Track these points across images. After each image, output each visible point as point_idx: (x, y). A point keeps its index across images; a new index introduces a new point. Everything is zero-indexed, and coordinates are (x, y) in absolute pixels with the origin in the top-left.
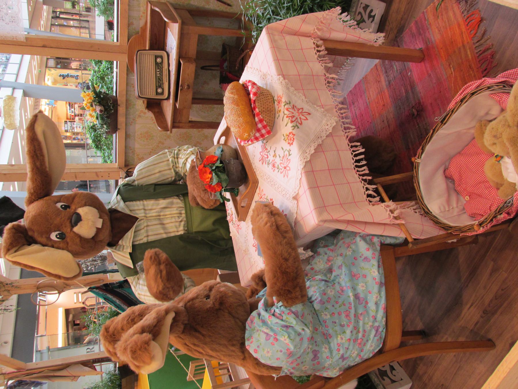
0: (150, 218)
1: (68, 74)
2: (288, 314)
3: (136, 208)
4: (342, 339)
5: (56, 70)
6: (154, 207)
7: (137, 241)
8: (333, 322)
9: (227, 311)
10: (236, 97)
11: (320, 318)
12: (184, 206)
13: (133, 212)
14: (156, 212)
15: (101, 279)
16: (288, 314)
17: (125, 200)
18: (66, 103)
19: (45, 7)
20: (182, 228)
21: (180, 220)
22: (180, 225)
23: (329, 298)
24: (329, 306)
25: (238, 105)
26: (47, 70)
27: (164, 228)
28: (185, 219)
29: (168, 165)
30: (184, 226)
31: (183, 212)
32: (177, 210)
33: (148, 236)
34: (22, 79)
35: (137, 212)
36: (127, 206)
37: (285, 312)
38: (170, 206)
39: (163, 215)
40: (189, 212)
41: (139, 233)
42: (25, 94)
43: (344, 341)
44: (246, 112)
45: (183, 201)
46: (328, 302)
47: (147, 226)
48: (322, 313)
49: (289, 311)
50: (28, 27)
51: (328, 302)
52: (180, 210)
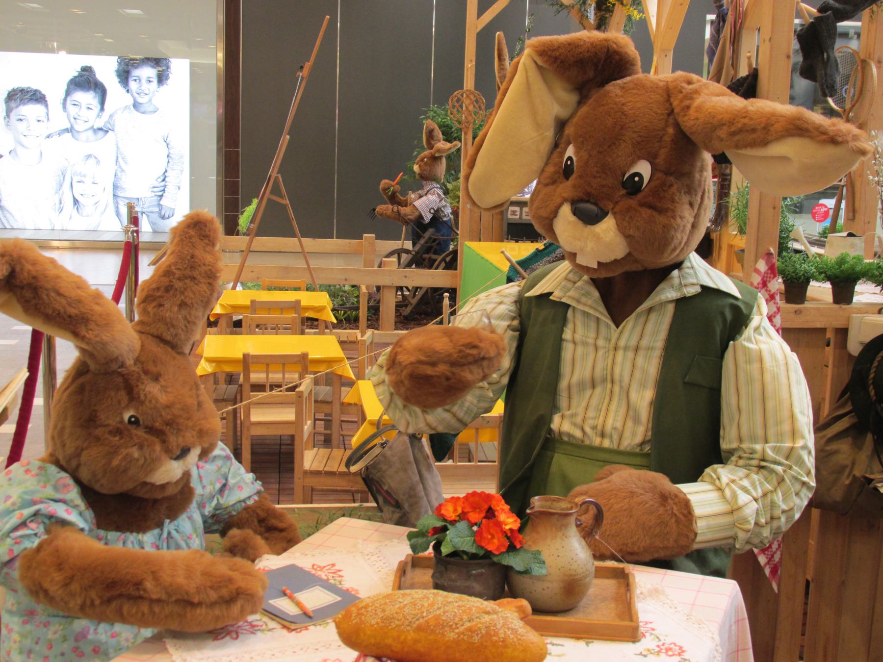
0: (611, 357)
2: (11, 551)
3: (650, 326)
4: (15, 642)
6: (638, 374)
7: (574, 316)
8: (39, 639)
9: (85, 445)
10: (452, 636)
11: (57, 619)
12: (622, 448)
13: (642, 320)
14: (621, 376)
15: (857, 216)
16: (11, 551)
17: (682, 303)
20: (566, 427)
21: (588, 429)
22: (575, 425)
23: (82, 655)
24: (66, 647)
25: (419, 629)
27: (581, 386)
28: (587, 442)
29: (754, 439)
30: (569, 435)
31: (606, 444)
32: (615, 428)
33: (574, 343)
35: (638, 329)
36: (663, 304)
37: (17, 546)
38: (631, 413)
39: (612, 391)
40: (602, 456)
41: (593, 325)
43: (12, 644)
44: (389, 641)
45: (638, 450)
46: (75, 650)
47: (596, 348)
48: (61, 627)
49: (16, 553)
51: (75, 650)
52: (611, 437)
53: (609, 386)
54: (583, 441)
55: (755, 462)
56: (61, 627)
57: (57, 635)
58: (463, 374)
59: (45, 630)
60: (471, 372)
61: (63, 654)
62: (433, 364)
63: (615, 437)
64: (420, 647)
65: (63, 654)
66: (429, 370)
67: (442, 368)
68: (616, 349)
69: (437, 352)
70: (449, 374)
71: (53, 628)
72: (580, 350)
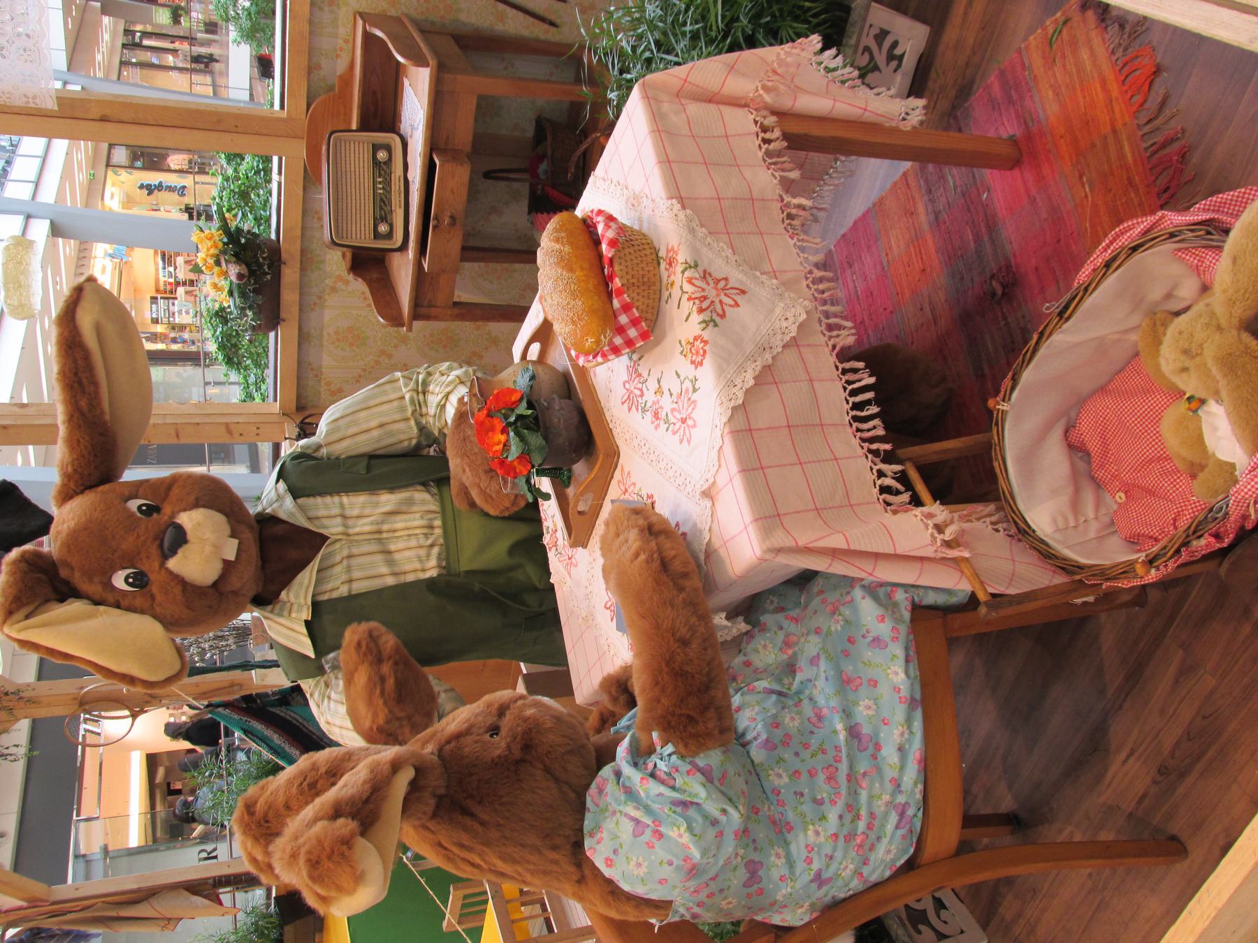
1: (161, 182)
2: (688, 773)
3: (322, 513)
5: (130, 173)
8: (795, 793)
10: (567, 249)
11: (765, 784)
12: (438, 509)
14: (372, 523)
16: (688, 773)
17: (295, 493)
18: (156, 253)
19: (106, 20)
20: (433, 562)
21: (429, 542)
22: (428, 555)
23: (787, 736)
24: (787, 755)
26: (110, 173)
27: (391, 563)
28: (441, 541)
30: (439, 558)
31: (438, 523)
32: (422, 517)
34: (48, 195)
35: (325, 522)
36: (302, 509)
37: (680, 769)
38: (404, 508)
39: (388, 531)
41: (329, 572)
42: (56, 231)
44: (591, 286)
45: (437, 497)
46: (785, 744)
47: (350, 557)
48: (770, 772)
50: (65, 69)
51: (785, 744)
52: (431, 520)
53: (385, 535)
54: (441, 545)
55: (421, 397)
56: (770, 772)
57: (781, 771)
58: (389, 649)
59: (782, 791)
60: (386, 642)
61: (797, 754)
62: (383, 679)
63: (430, 516)
64: (586, 266)
65: (797, 754)
66: (391, 682)
67: (386, 668)
68: (348, 535)
69: (369, 678)
70: (391, 662)
71: (777, 782)
72: (356, 575)
